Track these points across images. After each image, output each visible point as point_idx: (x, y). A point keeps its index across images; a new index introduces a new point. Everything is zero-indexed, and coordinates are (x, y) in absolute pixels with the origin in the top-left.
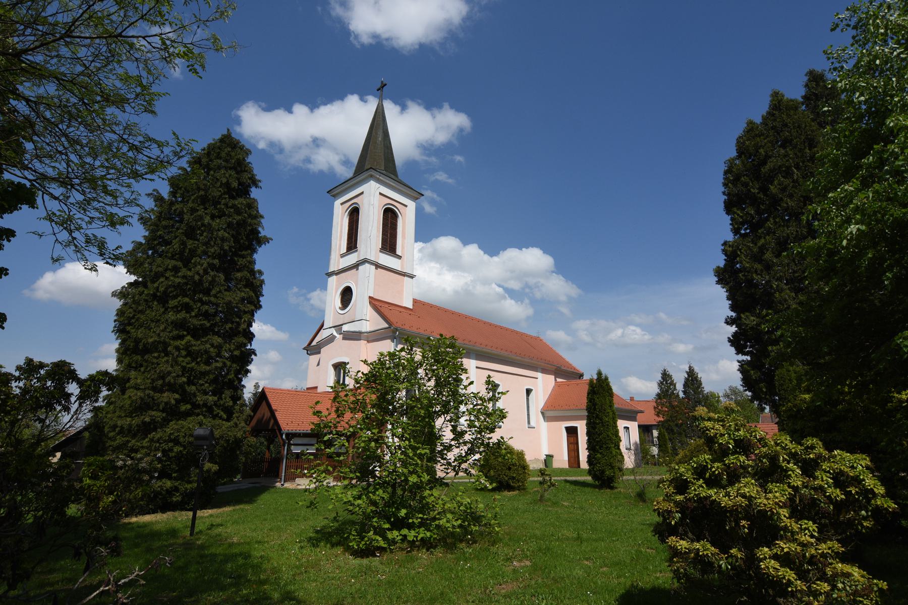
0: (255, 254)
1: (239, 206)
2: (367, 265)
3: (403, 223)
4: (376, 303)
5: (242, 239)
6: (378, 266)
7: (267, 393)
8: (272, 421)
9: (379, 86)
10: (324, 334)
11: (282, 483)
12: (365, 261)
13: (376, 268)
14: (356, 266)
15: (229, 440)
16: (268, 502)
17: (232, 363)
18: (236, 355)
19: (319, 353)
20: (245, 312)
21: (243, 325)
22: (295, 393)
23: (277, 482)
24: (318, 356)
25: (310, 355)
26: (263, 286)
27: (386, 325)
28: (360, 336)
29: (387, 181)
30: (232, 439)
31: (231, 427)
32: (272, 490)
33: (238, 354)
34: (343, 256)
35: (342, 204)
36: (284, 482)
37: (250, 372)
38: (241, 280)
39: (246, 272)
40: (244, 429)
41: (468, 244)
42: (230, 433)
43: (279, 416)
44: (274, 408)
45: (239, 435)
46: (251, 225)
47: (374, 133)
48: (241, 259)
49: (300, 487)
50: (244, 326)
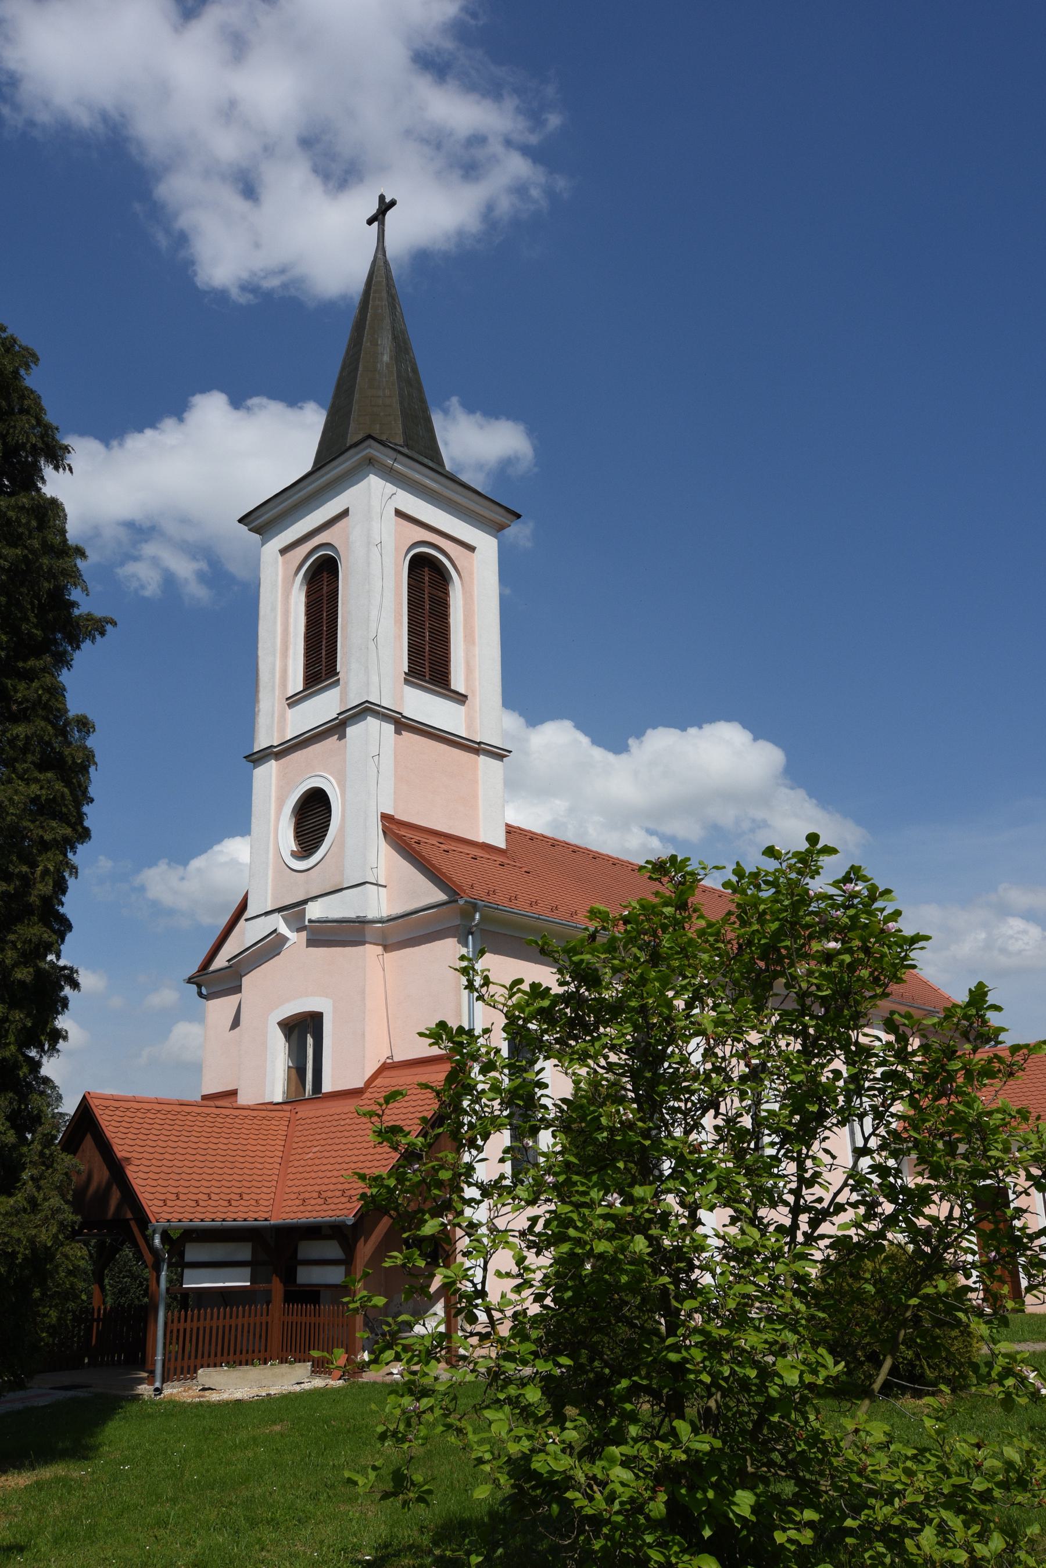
0: (65, 671)
1: (11, 514)
2: (371, 722)
3: (464, 592)
4: (402, 832)
5: (27, 620)
6: (402, 724)
7: (97, 1112)
8: (115, 1196)
9: (373, 208)
10: (248, 933)
11: (158, 1385)
12: (365, 710)
13: (398, 732)
14: (337, 728)
15: (14, 1254)
16: (139, 1453)
17: (10, 1008)
18: (22, 983)
19: (237, 989)
20: (44, 846)
21: (40, 886)
22: (178, 1108)
23: (141, 1381)
24: (239, 995)
25: (207, 998)
26: (92, 769)
27: (442, 897)
28: (362, 933)
29: (417, 476)
30: (23, 1251)
31: (18, 1213)
32: (134, 1408)
33: (28, 979)
34: (293, 701)
35: (284, 551)
36: (163, 1382)
37: (65, 1038)
38: (25, 750)
39: (43, 724)
40: (61, 1217)
41: (542, 721)
42: (15, 1232)
43: (135, 1176)
44: (120, 1152)
45: (45, 1237)
46: (51, 575)
47: (366, 343)
48: (22, 686)
49: (214, 1397)
50: (44, 888)
